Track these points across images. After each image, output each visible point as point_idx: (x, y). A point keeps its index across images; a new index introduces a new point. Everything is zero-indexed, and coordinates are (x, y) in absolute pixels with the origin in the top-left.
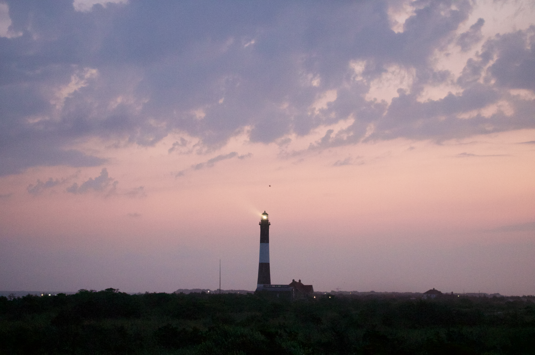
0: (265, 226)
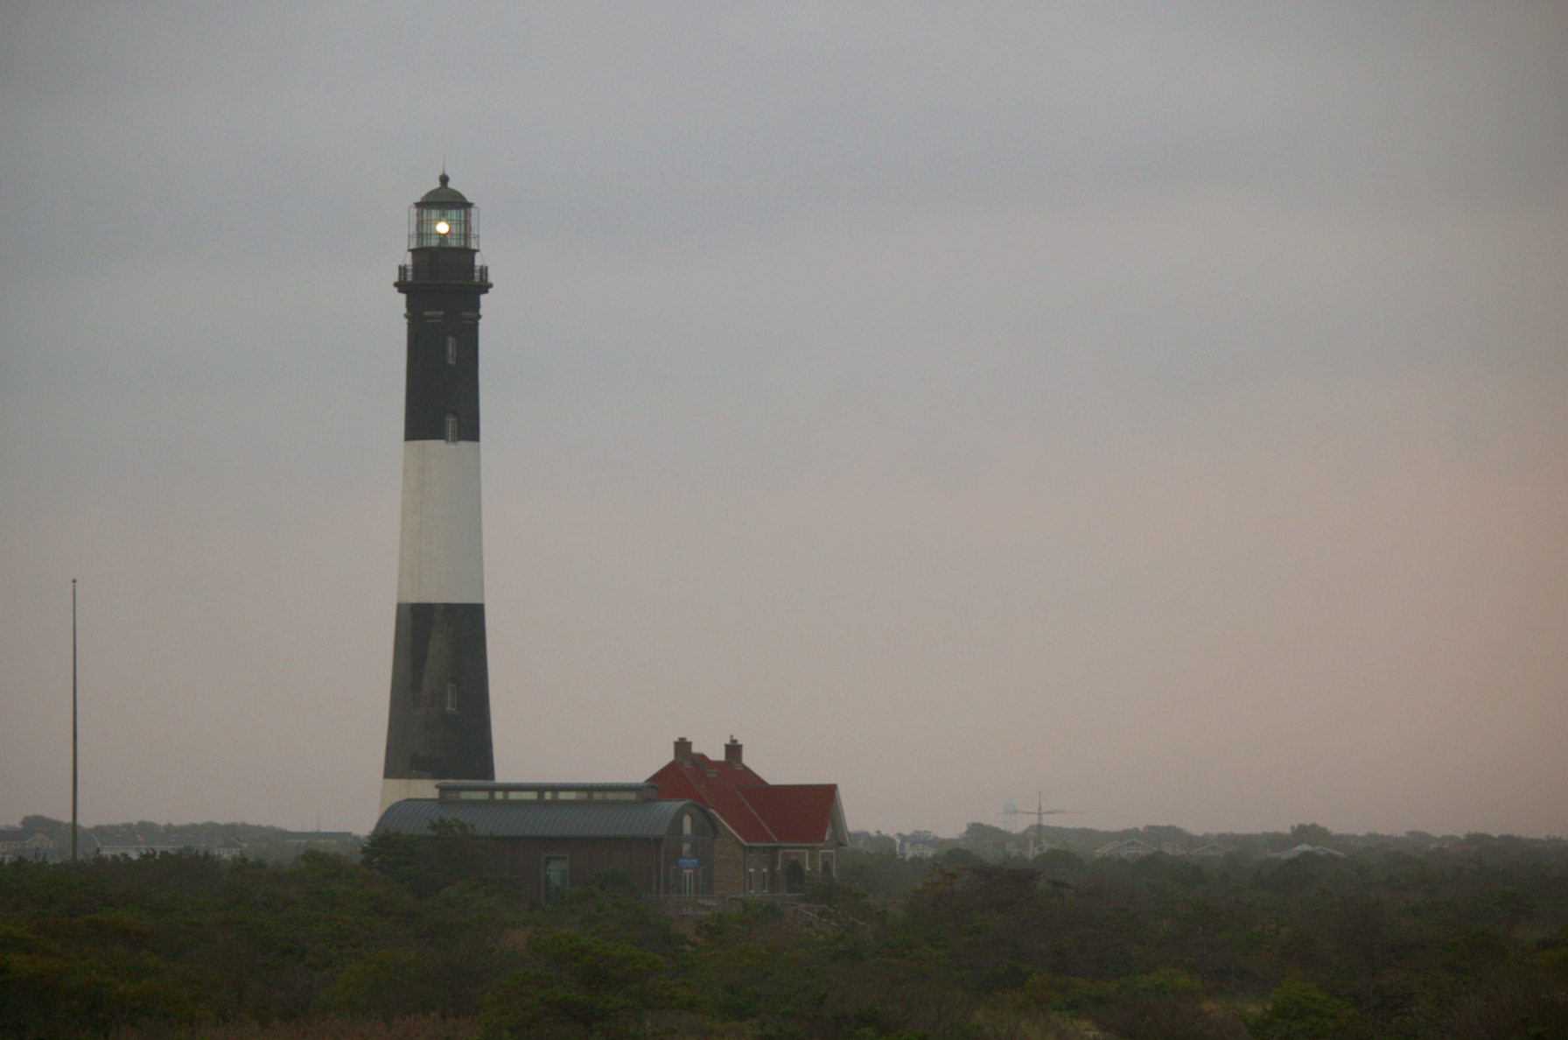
0: (443, 293)
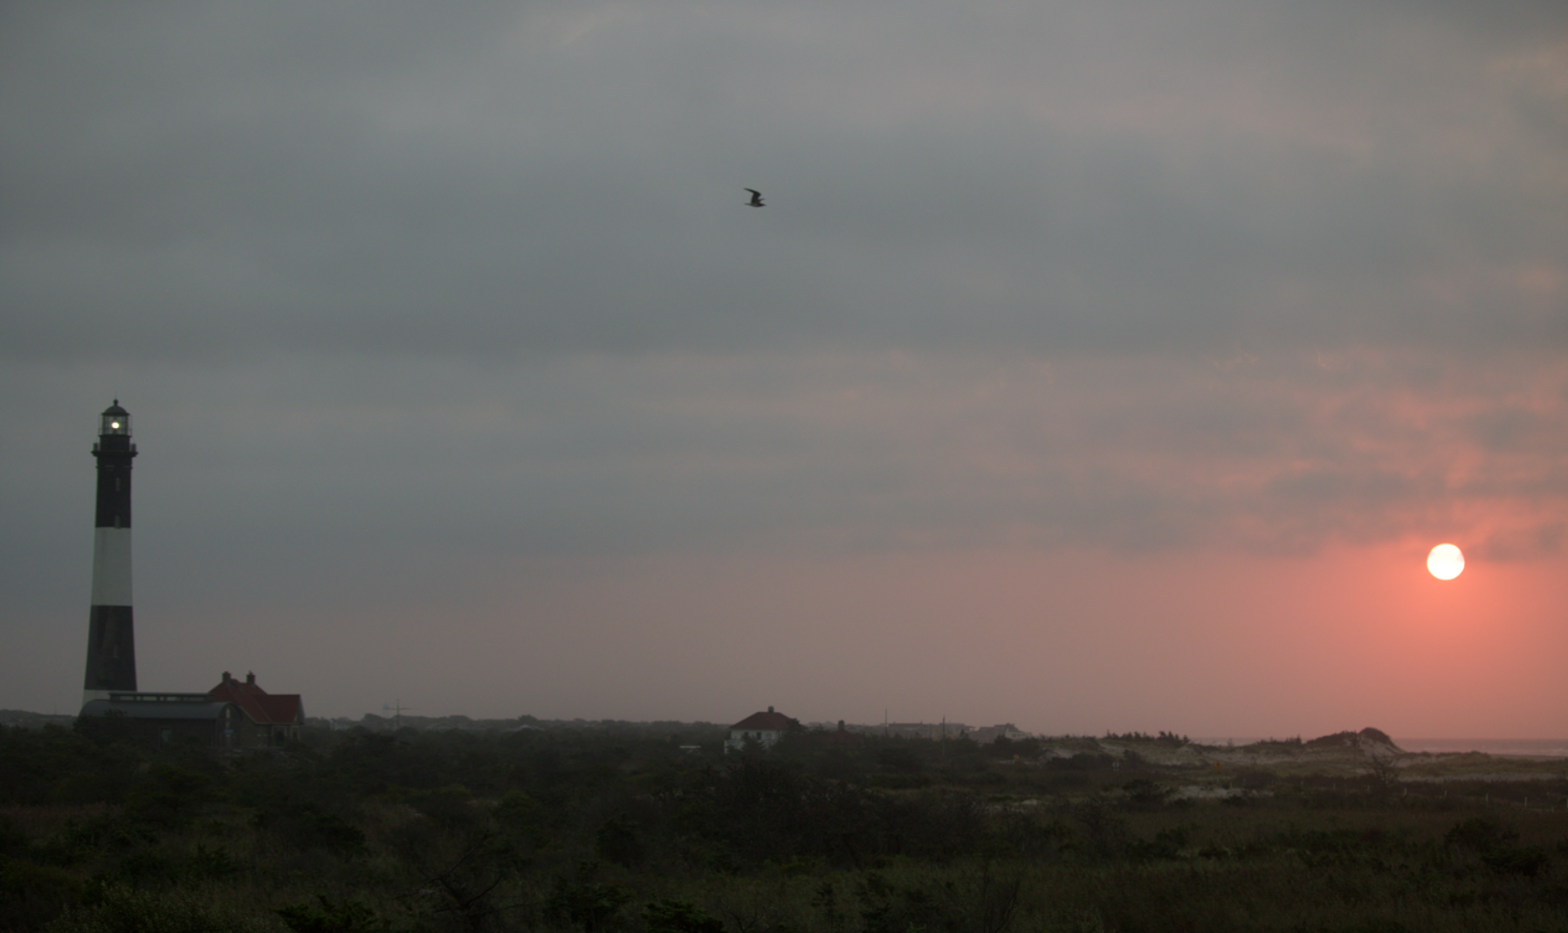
0: (115, 456)
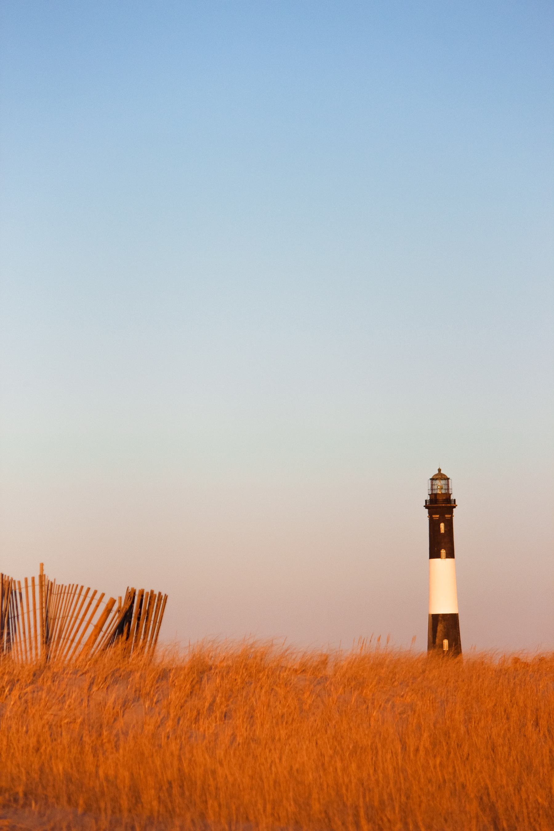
0: (440, 507)
